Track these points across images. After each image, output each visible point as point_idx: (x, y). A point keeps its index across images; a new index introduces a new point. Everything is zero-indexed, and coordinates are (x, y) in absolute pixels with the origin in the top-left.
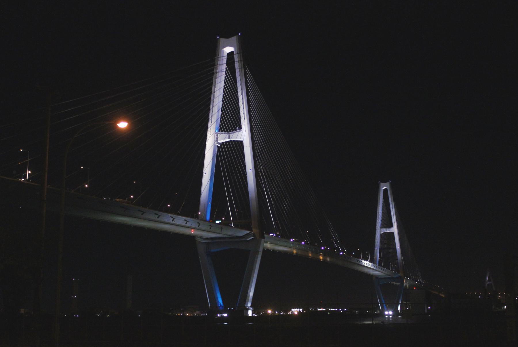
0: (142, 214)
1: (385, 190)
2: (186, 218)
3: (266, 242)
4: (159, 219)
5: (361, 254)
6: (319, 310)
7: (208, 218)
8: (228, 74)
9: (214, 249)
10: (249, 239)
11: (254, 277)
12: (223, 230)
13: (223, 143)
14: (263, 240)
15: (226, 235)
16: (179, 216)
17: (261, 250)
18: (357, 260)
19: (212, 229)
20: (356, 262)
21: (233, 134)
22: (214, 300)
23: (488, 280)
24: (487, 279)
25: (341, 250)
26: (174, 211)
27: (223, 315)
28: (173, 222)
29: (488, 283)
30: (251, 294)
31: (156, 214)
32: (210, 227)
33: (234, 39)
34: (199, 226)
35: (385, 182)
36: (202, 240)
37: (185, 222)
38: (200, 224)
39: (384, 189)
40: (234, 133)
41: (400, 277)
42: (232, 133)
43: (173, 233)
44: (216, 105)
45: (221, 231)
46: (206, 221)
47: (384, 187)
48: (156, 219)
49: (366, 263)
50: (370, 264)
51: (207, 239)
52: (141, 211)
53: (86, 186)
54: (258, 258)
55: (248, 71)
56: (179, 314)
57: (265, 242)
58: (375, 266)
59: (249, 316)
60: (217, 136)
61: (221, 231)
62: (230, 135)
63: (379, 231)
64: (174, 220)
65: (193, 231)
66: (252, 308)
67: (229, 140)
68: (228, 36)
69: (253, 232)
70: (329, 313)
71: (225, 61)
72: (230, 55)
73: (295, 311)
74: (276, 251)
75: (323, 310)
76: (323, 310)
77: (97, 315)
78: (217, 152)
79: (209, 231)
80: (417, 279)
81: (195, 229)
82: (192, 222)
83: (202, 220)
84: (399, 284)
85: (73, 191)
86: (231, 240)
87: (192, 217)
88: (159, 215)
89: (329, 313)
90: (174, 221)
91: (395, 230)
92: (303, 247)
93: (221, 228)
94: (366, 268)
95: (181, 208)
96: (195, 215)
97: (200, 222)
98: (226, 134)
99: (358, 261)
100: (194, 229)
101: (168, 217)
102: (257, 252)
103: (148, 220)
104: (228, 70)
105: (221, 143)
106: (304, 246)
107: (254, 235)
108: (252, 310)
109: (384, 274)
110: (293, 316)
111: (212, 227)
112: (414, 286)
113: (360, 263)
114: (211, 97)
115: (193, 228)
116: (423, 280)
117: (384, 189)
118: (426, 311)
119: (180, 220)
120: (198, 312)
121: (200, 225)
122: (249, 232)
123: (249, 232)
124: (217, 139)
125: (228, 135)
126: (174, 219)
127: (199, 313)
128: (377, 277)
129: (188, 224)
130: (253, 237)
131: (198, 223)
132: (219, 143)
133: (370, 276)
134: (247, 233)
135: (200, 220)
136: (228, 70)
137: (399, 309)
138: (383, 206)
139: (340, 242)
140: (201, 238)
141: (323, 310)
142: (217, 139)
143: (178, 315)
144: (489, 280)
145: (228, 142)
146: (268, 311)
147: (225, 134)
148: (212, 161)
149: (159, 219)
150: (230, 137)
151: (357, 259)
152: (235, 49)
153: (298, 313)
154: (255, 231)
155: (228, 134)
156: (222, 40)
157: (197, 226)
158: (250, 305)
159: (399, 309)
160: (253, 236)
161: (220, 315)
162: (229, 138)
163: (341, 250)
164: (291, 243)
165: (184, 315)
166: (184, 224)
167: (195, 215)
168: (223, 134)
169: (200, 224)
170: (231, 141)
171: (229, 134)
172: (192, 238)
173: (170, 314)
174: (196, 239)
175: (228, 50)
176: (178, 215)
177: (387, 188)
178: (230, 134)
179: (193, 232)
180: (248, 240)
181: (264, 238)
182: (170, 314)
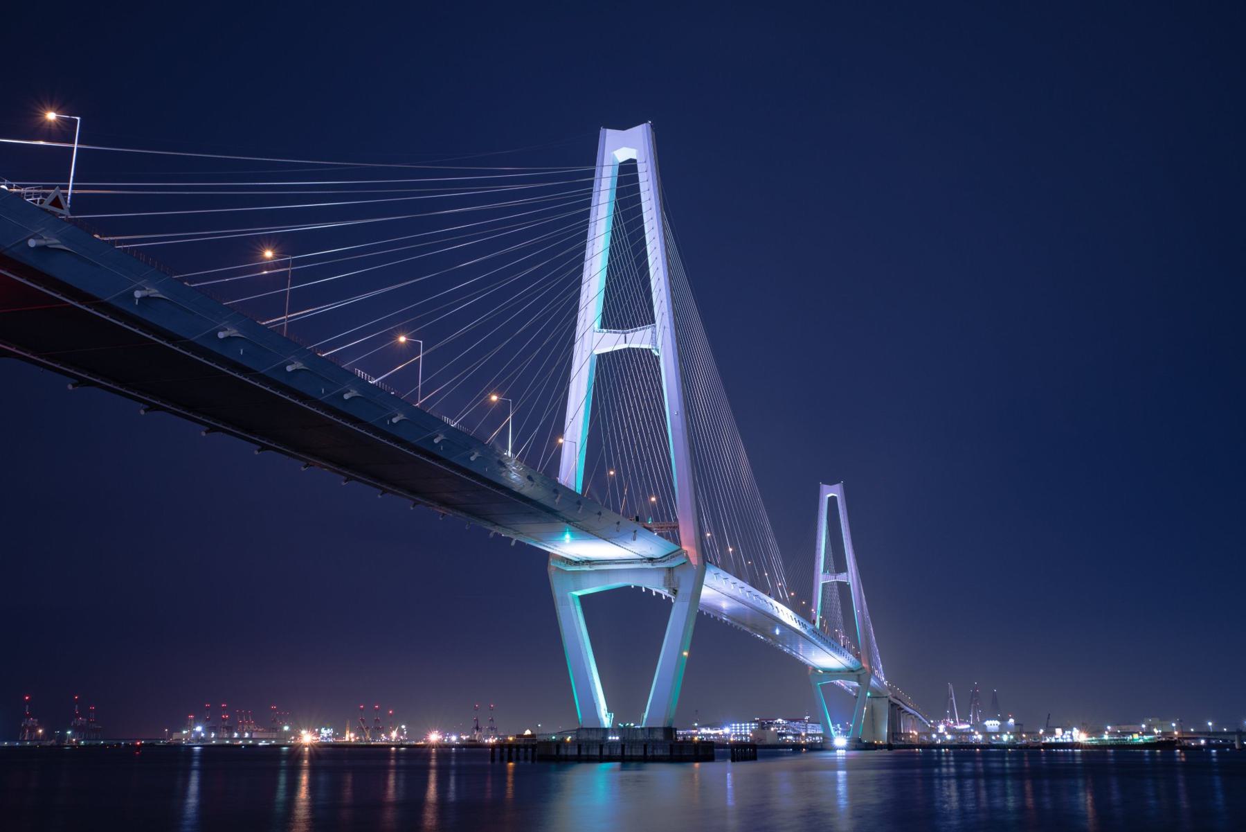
1: (833, 501)
25: (865, 709)
35: (831, 482)
40: (636, 330)
42: (632, 332)
44: (649, 734)
47: (830, 492)
67: (625, 346)
78: (595, 383)
91: (851, 576)
104: (433, 777)
114: (647, 261)
117: (829, 498)
125: (623, 335)
136: (433, 777)
145: (625, 350)
147: (616, 333)
148: (571, 379)
155: (623, 333)
163: (865, 709)
170: (629, 349)
177: (835, 495)
178: (628, 333)
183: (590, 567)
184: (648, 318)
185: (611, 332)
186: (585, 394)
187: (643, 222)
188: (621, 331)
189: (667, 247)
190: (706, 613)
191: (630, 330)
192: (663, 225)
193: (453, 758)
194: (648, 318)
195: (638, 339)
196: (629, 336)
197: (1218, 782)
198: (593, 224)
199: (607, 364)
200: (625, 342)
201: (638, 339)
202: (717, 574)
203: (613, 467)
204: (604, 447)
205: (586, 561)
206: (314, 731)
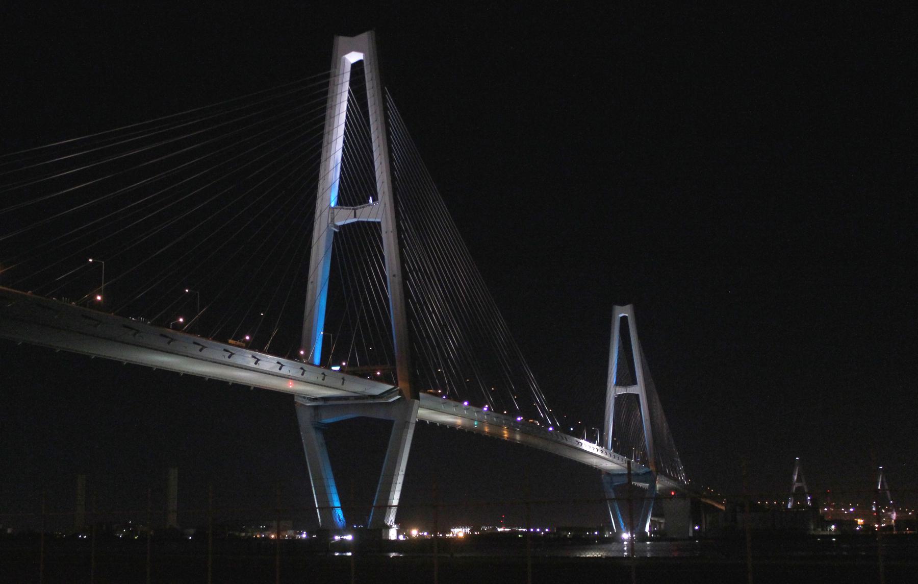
0: (201, 350)
2: (282, 360)
3: (420, 406)
4: (231, 360)
5: (585, 430)
6: (500, 530)
7: (317, 360)
8: (354, 102)
9: (328, 419)
10: (391, 400)
11: (401, 470)
12: (345, 381)
13: (343, 226)
14: (416, 401)
15: (351, 392)
16: (267, 355)
17: (413, 420)
18: (577, 441)
19: (326, 382)
20: (574, 445)
21: (361, 209)
22: (327, 509)
23: (797, 480)
24: (795, 478)
25: (550, 422)
26: (257, 346)
27: (345, 537)
28: (257, 366)
29: (797, 485)
30: (395, 499)
31: (226, 350)
32: (323, 375)
33: (365, 38)
34: (303, 374)
36: (307, 401)
37: (301, 373)
38: (304, 371)
39: (622, 318)
40: (364, 207)
41: (650, 473)
42: (360, 208)
43: (254, 388)
45: (343, 384)
46: (313, 365)
47: (622, 312)
48: (226, 360)
49: (586, 445)
50: (599, 448)
51: (316, 399)
52: (199, 344)
53: (99, 298)
54: (408, 435)
55: (389, 97)
56: (258, 536)
57: (421, 407)
58: (608, 454)
59: (391, 540)
60: (334, 213)
61: (343, 384)
62: (357, 211)
63: (614, 391)
64: (259, 363)
65: (291, 384)
66: (397, 526)
68: (352, 31)
69: (399, 388)
70: (520, 536)
71: (347, 77)
72: (357, 68)
73: (459, 532)
74: (426, 422)
75: (506, 530)
76: (506, 530)
77: (118, 535)
79: (321, 385)
80: (677, 476)
81: (295, 380)
82: (290, 368)
83: (308, 363)
84: (648, 485)
85: (73, 303)
86: (361, 402)
87: (291, 357)
88: (203, 346)
89: (520, 536)
90: (258, 364)
91: (638, 389)
92: (495, 419)
93: (343, 379)
94: (592, 456)
95: (448, 386)
96: (171, 323)
97: (306, 367)
98: (350, 209)
99: (579, 443)
100: (293, 381)
101: (246, 358)
102: (406, 424)
103: (211, 361)
105: (340, 226)
106: (487, 415)
107: (400, 393)
108: (397, 530)
109: (622, 467)
110: (455, 540)
111: (305, 372)
112: (672, 489)
113: (579, 446)
115: (291, 379)
116: (687, 479)
117: (621, 317)
118: (691, 534)
119: (269, 362)
120: (291, 532)
121: (283, 367)
122: (391, 387)
123: (391, 387)
124: (333, 220)
125: (353, 211)
126: (258, 360)
127: (293, 534)
128: (608, 473)
129: (284, 371)
130: (398, 397)
131: (302, 368)
132: (336, 226)
133: (595, 472)
134: (388, 389)
135: (305, 363)
137: (647, 529)
138: (619, 348)
139: (549, 410)
140: (304, 398)
141: (506, 530)
142: (334, 219)
143: (256, 536)
144: (799, 480)
145: (352, 224)
146: (414, 529)
147: (347, 209)
149: (231, 360)
150: (358, 214)
151: (577, 439)
152: (365, 56)
153: (466, 534)
154: (403, 385)
155: (353, 209)
156: (342, 41)
157: (320, 380)
158: (393, 520)
159: (647, 529)
160: (399, 395)
161: (339, 538)
162: (355, 217)
164: (464, 409)
165: (267, 539)
166: (276, 370)
167: (171, 323)
168: (344, 209)
169: (304, 371)
170: (358, 222)
171: (355, 210)
172: (287, 398)
173: (243, 534)
174: (295, 400)
175: (353, 57)
176: (264, 352)
177: (627, 315)
178: (357, 209)
179: (291, 386)
180: (389, 403)
181: (418, 398)
182: (243, 534)
186: (324, 253)
189: (619, 341)
191: (359, 207)
192: (641, 354)
193: (625, 549)
194: (634, 382)
195: (632, 390)
198: (325, 148)
200: (355, 217)
201: (632, 390)
202: (457, 406)
203: (600, 423)
205: (369, 396)
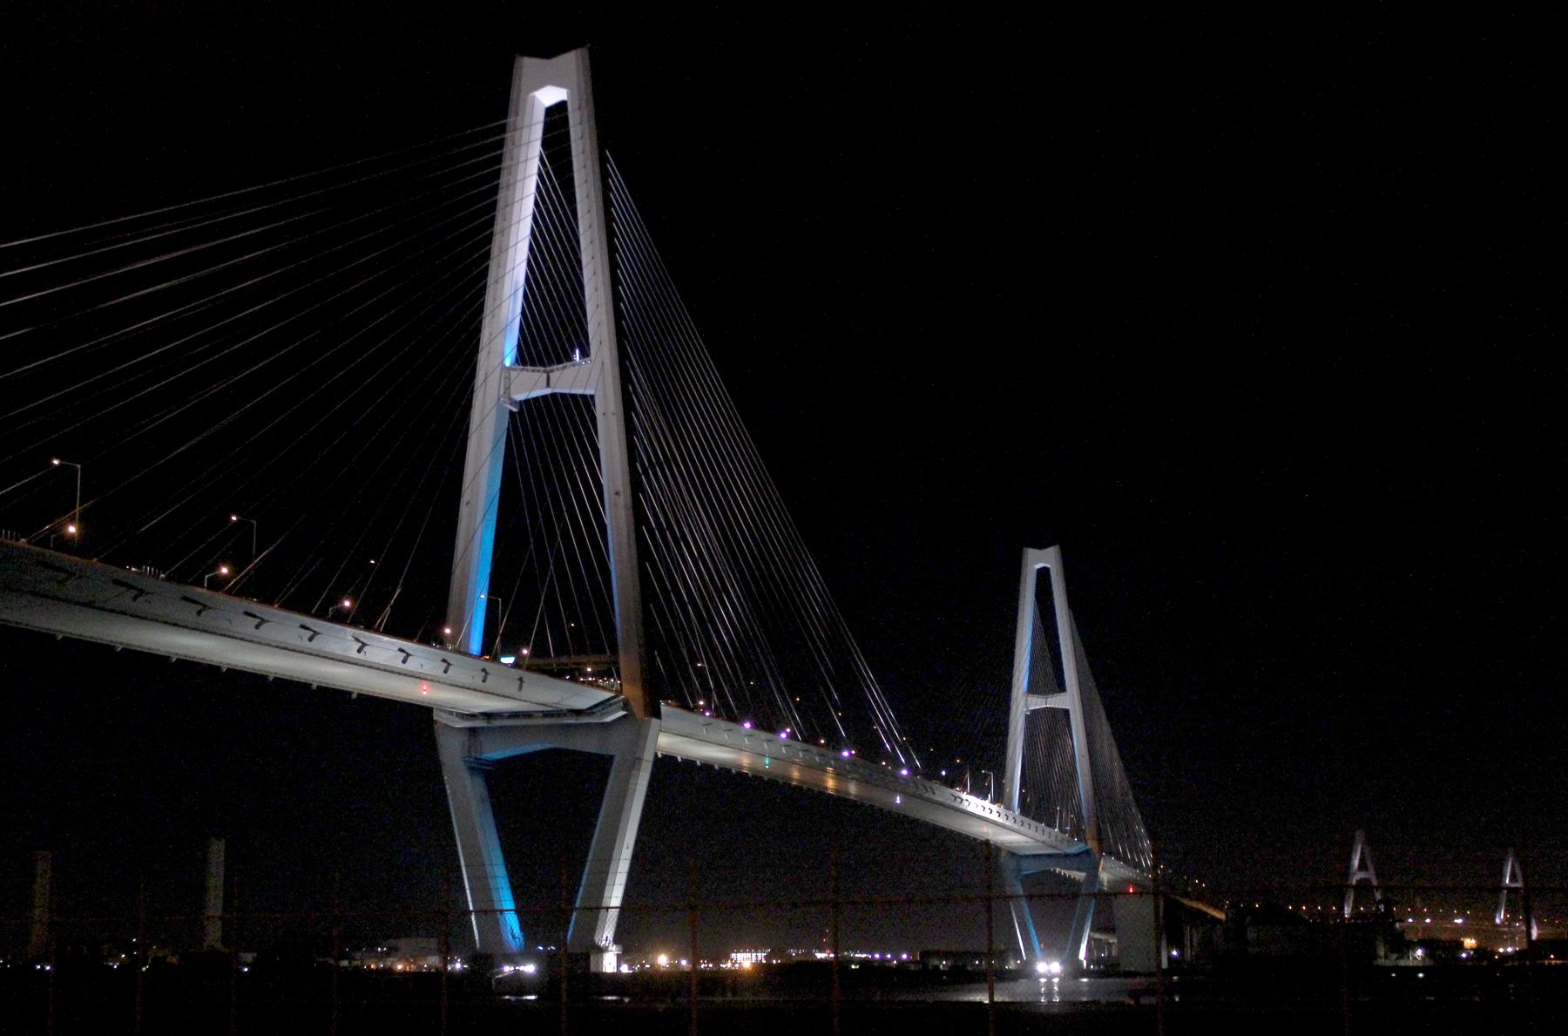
40: (565, 368)
67: (548, 391)
125: (545, 375)
145: (544, 397)
147: (533, 371)
155: (545, 371)
170: (554, 395)
178: (552, 371)
183: (577, 720)
184: (1061, 687)
185: (527, 370)
187: (569, 140)
188: (542, 369)
190: (662, 754)
191: (555, 367)
194: (1061, 687)
195: (1057, 702)
196: (1049, 700)
197: (471, 908)
199: (1033, 718)
201: (1057, 702)
204: (552, 567)
206: (1465, 913)
